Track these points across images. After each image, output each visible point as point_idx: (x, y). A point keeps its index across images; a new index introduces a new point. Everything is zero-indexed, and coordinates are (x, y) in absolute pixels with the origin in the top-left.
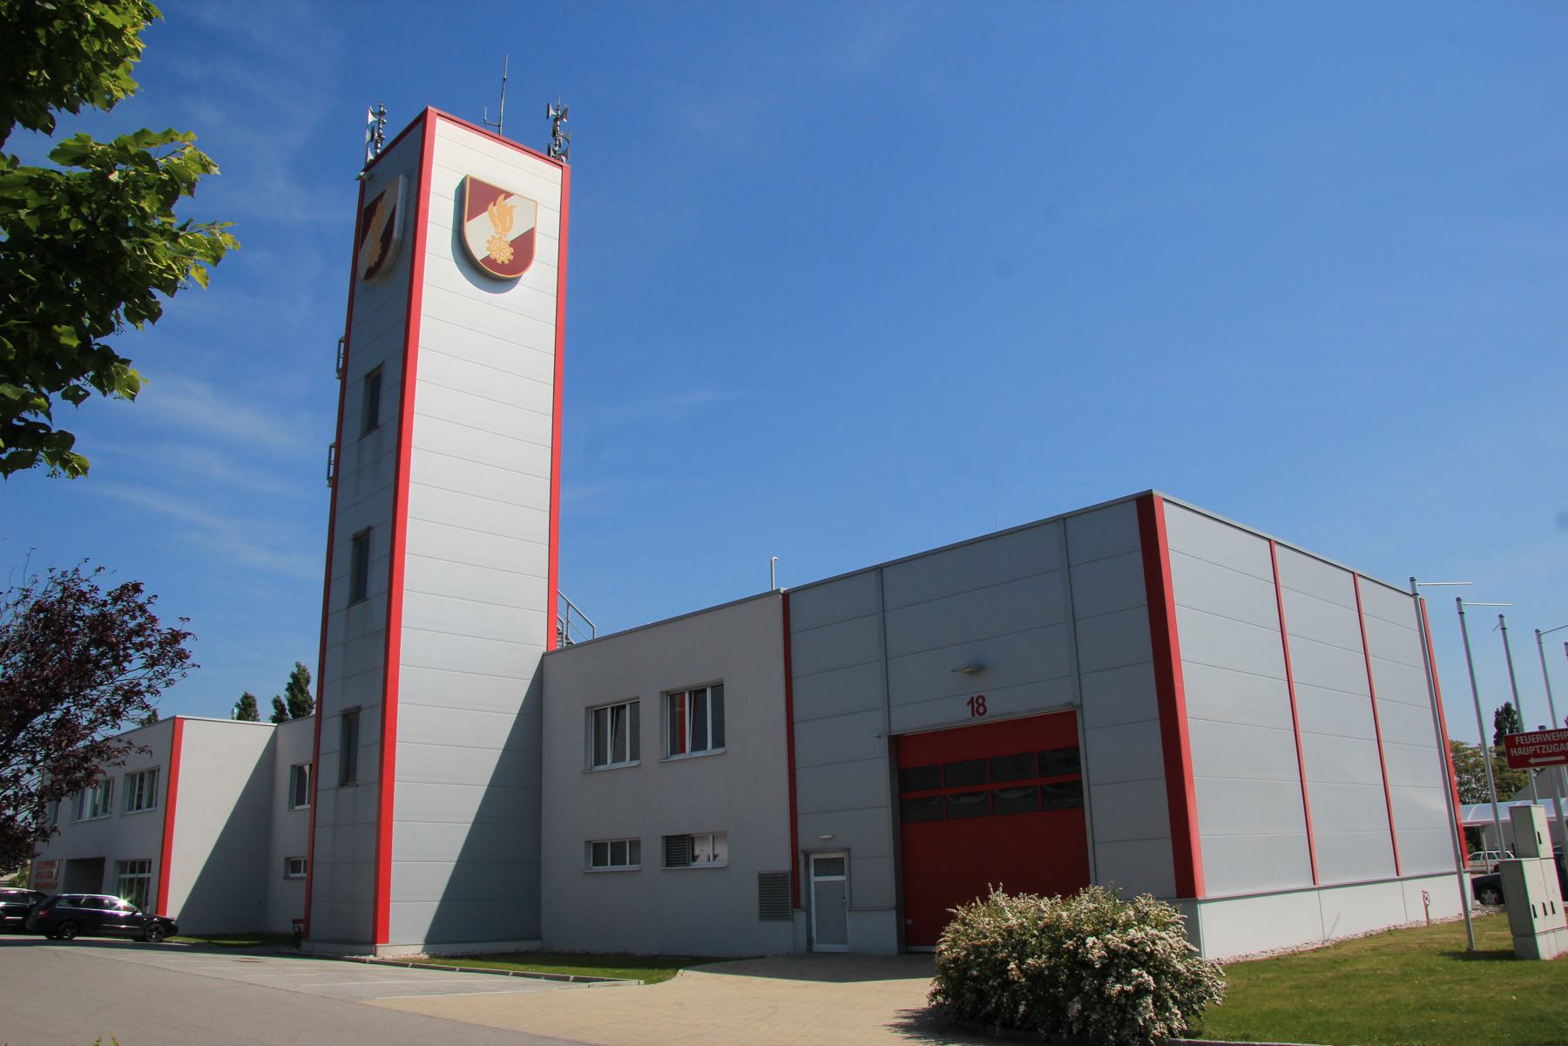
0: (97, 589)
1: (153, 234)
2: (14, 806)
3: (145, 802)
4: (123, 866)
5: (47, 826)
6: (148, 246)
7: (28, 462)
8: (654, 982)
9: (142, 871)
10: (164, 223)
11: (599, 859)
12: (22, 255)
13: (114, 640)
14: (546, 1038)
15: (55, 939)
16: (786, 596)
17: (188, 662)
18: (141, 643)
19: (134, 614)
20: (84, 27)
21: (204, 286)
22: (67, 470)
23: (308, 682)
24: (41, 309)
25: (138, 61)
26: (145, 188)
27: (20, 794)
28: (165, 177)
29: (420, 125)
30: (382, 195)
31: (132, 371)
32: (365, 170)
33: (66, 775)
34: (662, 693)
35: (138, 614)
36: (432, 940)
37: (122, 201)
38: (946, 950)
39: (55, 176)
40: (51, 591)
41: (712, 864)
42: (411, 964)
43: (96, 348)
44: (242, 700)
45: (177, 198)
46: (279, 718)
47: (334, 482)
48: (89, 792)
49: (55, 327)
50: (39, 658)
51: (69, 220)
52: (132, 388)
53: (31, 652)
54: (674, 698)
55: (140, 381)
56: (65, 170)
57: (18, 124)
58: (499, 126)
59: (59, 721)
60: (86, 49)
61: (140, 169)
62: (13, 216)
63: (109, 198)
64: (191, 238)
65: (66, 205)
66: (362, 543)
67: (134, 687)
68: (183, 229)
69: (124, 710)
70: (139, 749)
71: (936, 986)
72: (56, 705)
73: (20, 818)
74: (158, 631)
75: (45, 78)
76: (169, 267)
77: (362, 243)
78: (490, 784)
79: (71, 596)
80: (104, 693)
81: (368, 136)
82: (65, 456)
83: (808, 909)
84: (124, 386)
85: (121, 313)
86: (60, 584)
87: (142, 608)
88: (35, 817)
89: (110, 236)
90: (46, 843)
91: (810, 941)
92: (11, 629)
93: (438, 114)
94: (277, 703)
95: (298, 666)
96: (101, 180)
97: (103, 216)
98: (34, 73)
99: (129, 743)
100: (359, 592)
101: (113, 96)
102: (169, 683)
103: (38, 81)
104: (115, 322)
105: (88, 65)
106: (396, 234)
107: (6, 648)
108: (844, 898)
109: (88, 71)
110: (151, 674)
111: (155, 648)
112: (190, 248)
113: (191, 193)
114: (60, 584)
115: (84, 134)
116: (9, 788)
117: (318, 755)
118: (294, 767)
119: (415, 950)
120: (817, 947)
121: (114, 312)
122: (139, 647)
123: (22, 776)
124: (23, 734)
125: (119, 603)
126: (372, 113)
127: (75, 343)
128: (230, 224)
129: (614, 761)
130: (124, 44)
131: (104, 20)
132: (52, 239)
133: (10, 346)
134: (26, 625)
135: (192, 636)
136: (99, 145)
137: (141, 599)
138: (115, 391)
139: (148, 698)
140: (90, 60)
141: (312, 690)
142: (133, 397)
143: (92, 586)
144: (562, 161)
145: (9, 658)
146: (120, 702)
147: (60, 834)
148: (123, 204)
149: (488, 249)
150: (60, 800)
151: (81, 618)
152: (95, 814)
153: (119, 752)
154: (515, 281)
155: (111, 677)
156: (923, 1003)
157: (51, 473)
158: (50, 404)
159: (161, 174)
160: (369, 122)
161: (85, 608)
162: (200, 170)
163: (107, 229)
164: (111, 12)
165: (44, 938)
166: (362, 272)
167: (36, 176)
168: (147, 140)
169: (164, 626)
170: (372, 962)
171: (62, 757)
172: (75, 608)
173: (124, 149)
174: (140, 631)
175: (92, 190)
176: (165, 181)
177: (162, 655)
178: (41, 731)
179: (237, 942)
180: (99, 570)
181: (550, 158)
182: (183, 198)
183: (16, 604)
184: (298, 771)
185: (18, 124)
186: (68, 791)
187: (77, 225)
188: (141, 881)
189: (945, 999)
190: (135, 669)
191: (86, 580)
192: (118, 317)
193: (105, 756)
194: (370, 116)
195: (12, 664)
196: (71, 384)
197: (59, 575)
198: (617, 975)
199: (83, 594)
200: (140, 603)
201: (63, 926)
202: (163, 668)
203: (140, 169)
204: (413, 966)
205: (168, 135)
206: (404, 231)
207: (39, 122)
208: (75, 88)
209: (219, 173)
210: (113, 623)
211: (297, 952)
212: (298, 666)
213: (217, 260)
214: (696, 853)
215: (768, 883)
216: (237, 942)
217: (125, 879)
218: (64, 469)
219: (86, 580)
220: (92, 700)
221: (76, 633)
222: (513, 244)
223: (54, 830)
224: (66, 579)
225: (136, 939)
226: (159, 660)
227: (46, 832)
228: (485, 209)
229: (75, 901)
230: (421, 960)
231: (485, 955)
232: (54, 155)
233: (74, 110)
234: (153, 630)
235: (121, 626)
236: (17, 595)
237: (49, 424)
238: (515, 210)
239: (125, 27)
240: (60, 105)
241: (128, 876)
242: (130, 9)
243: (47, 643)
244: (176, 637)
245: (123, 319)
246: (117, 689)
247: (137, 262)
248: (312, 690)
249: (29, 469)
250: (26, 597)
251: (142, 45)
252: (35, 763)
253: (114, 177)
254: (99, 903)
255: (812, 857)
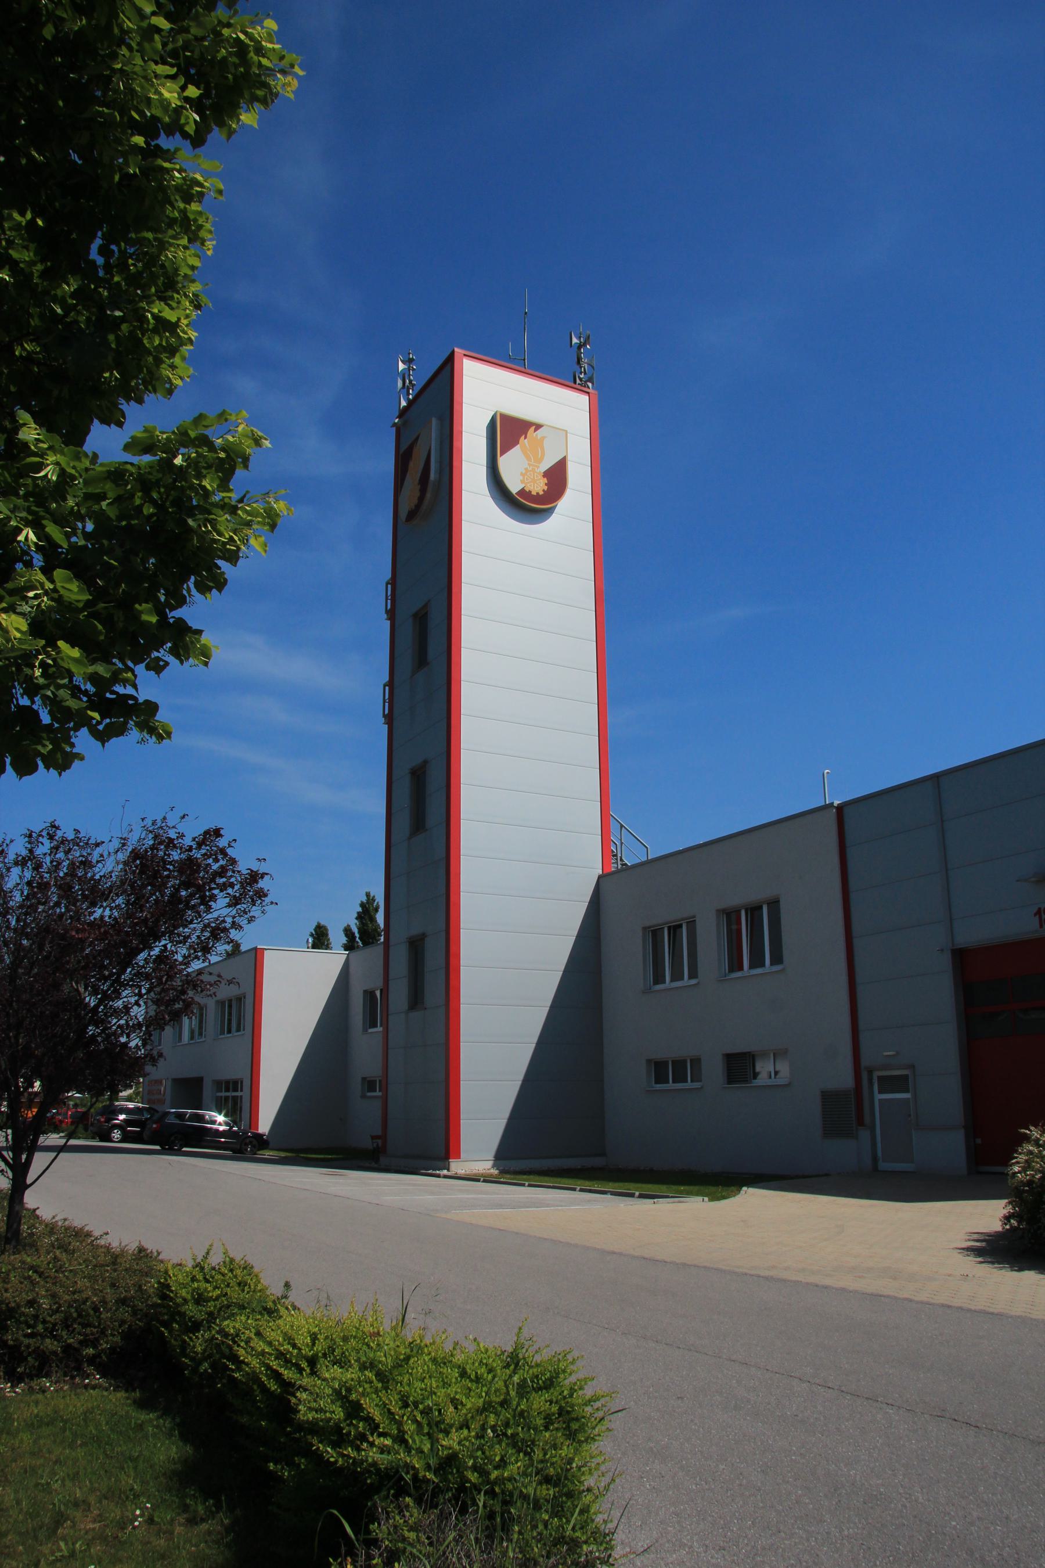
0: (183, 835)
1: (215, 510)
2: (127, 1034)
3: (234, 1028)
4: (219, 1085)
5: (155, 1053)
6: (211, 521)
7: (120, 730)
8: (718, 1199)
9: (236, 1090)
10: (224, 497)
11: (661, 1078)
12: (105, 542)
13: (201, 882)
14: (614, 1253)
15: (167, 1149)
16: (840, 809)
17: (267, 900)
18: (224, 884)
19: (216, 857)
20: (146, 326)
21: (263, 554)
22: (153, 737)
23: (377, 910)
24: (123, 590)
25: (192, 348)
26: (206, 468)
27: (131, 1023)
28: (222, 455)
29: (448, 367)
30: (417, 439)
31: (205, 639)
32: (400, 417)
33: (167, 1007)
34: (718, 911)
35: (220, 857)
36: (502, 1155)
37: (186, 482)
38: (1019, 1172)
39: (129, 467)
40: (144, 839)
41: (769, 1082)
42: (482, 1179)
43: (171, 621)
44: (315, 930)
45: (234, 473)
46: (350, 946)
47: (389, 719)
48: (186, 1020)
49: (137, 606)
50: (137, 902)
51: (142, 505)
52: (205, 654)
53: (131, 894)
54: (730, 916)
55: (212, 648)
56: (135, 460)
57: (96, 422)
58: (524, 360)
59: (158, 957)
60: (147, 345)
61: (200, 450)
62: (96, 507)
63: (175, 481)
64: (248, 508)
65: (139, 492)
66: (419, 776)
67: (220, 924)
68: (241, 501)
69: (213, 946)
70: (228, 981)
71: (1009, 1209)
72: (155, 942)
73: (132, 1044)
74: (239, 872)
75: (116, 377)
76: (231, 539)
77: (401, 487)
78: (551, 1005)
79: (161, 843)
80: (194, 931)
81: (400, 384)
82: (151, 724)
83: (872, 1128)
84: (199, 655)
85: (192, 586)
86: (151, 832)
87: (223, 851)
88: (144, 1045)
89: (178, 516)
90: (155, 1068)
91: (875, 1159)
92: (113, 875)
93: (465, 355)
94: (348, 932)
95: (368, 895)
96: (167, 464)
97: (171, 498)
98: (107, 375)
99: (219, 976)
100: (418, 824)
101: (171, 384)
102: (251, 920)
103: (111, 382)
104: (187, 595)
105: (150, 359)
106: (433, 476)
107: (110, 892)
108: (910, 1115)
109: (150, 365)
110: (234, 912)
111: (236, 887)
112: (249, 518)
113: (246, 467)
114: (151, 832)
115: (149, 425)
116: (121, 1019)
117: (388, 981)
118: (365, 992)
119: (485, 1166)
120: (883, 1166)
121: (185, 586)
122: (223, 888)
123: (131, 1008)
124: (129, 969)
125: (203, 847)
126: (402, 361)
127: (154, 619)
128: (283, 492)
129: (673, 980)
130: (179, 335)
131: (162, 317)
132: (129, 525)
133: (100, 627)
134: (126, 870)
135: (269, 876)
136: (163, 433)
137: (222, 843)
138: (191, 660)
139: (234, 934)
140: (152, 355)
141: (380, 918)
142: (206, 664)
143: (179, 833)
144: (588, 387)
145: (114, 901)
146: (209, 938)
147: (165, 1060)
148: (187, 485)
149: (522, 482)
150: (163, 1029)
151: (170, 863)
152: (192, 1037)
153: (211, 985)
154: (550, 511)
155: (200, 916)
156: (997, 1226)
157: (140, 740)
158: (135, 676)
159: (218, 453)
160: (400, 370)
161: (174, 853)
162: (253, 445)
163: (175, 509)
164: (167, 308)
165: (158, 1147)
166: (403, 514)
167: (113, 469)
168: (205, 423)
169: (244, 866)
170: (445, 1177)
171: (163, 990)
172: (165, 854)
173: (185, 434)
174: (222, 872)
175: (160, 475)
176: (222, 458)
177: (244, 894)
178: (143, 967)
179: (322, 1156)
180: (184, 817)
181: (577, 386)
182: (240, 473)
183: (117, 852)
184: (369, 995)
185: (96, 422)
186: (170, 1020)
187: (148, 510)
188: (235, 1098)
189: (1019, 1222)
190: (220, 908)
191: (174, 827)
192: (189, 590)
193: (199, 989)
194: (400, 364)
195: (116, 906)
196: (153, 656)
197: (150, 824)
198: (681, 1192)
199: (171, 840)
200: (221, 847)
201: (172, 1138)
202: (245, 906)
203: (200, 450)
204: (485, 1181)
205: (222, 416)
206: (440, 472)
207: (114, 418)
208: (140, 381)
209: (270, 446)
210: (199, 866)
211: (376, 1166)
212: (368, 895)
213: (273, 526)
214: (758, 1069)
215: (830, 1099)
216: (322, 1156)
217: (221, 1097)
218: (151, 737)
219: (174, 827)
220: (184, 936)
221: (168, 877)
222: (547, 474)
223: (160, 1055)
224: (156, 827)
225: (234, 1152)
226: (240, 899)
227: (154, 1057)
228: (516, 443)
229: (180, 1116)
230: (491, 1175)
231: (552, 1171)
232: (127, 448)
233: (140, 401)
234: (234, 872)
235: (206, 868)
236: (116, 844)
237: (135, 694)
238: (545, 442)
239: (179, 319)
240: (128, 399)
241: (224, 1094)
242: (182, 302)
243: (144, 886)
244: (254, 877)
245: (194, 591)
246: (206, 926)
247: (202, 537)
248: (380, 918)
249: (122, 737)
250: (124, 845)
251: (193, 333)
252: (140, 995)
253: (178, 461)
254: (201, 1118)
255: (876, 1074)
